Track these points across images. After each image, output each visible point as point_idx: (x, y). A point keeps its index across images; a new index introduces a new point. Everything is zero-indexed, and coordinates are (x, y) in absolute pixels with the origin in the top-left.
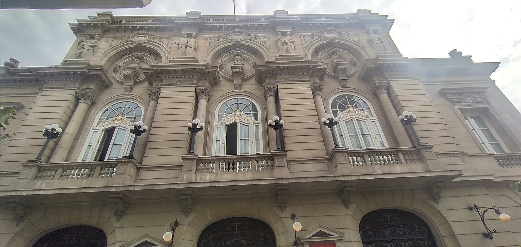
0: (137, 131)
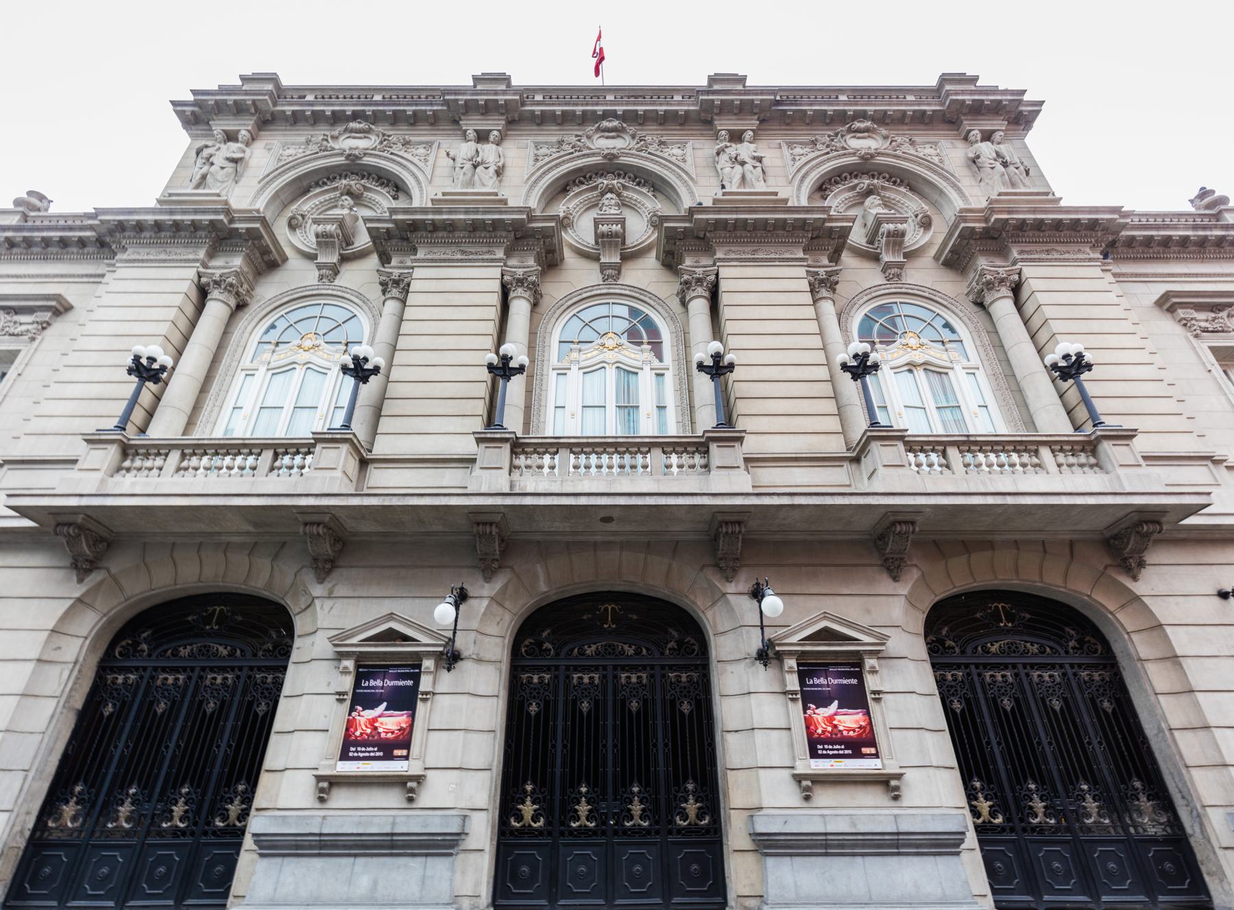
0: (359, 371)
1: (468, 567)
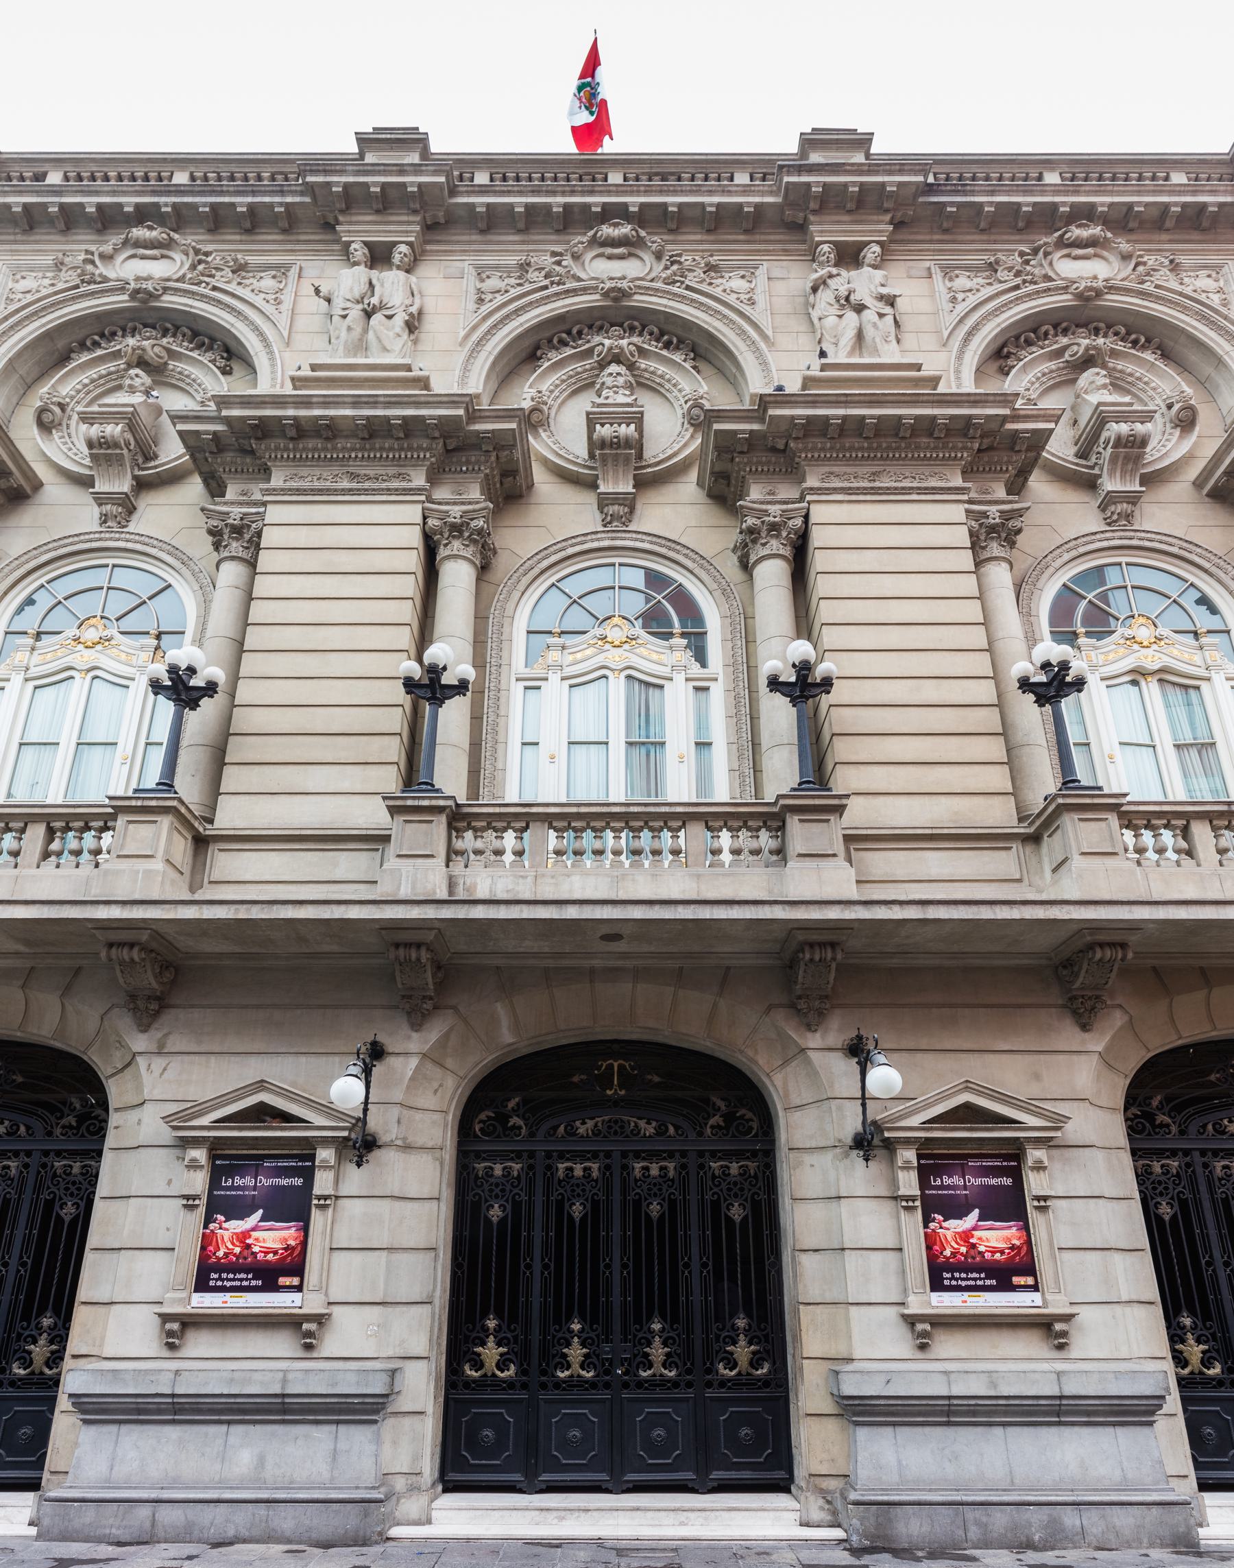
0: (182, 690)
1: (383, 1007)
